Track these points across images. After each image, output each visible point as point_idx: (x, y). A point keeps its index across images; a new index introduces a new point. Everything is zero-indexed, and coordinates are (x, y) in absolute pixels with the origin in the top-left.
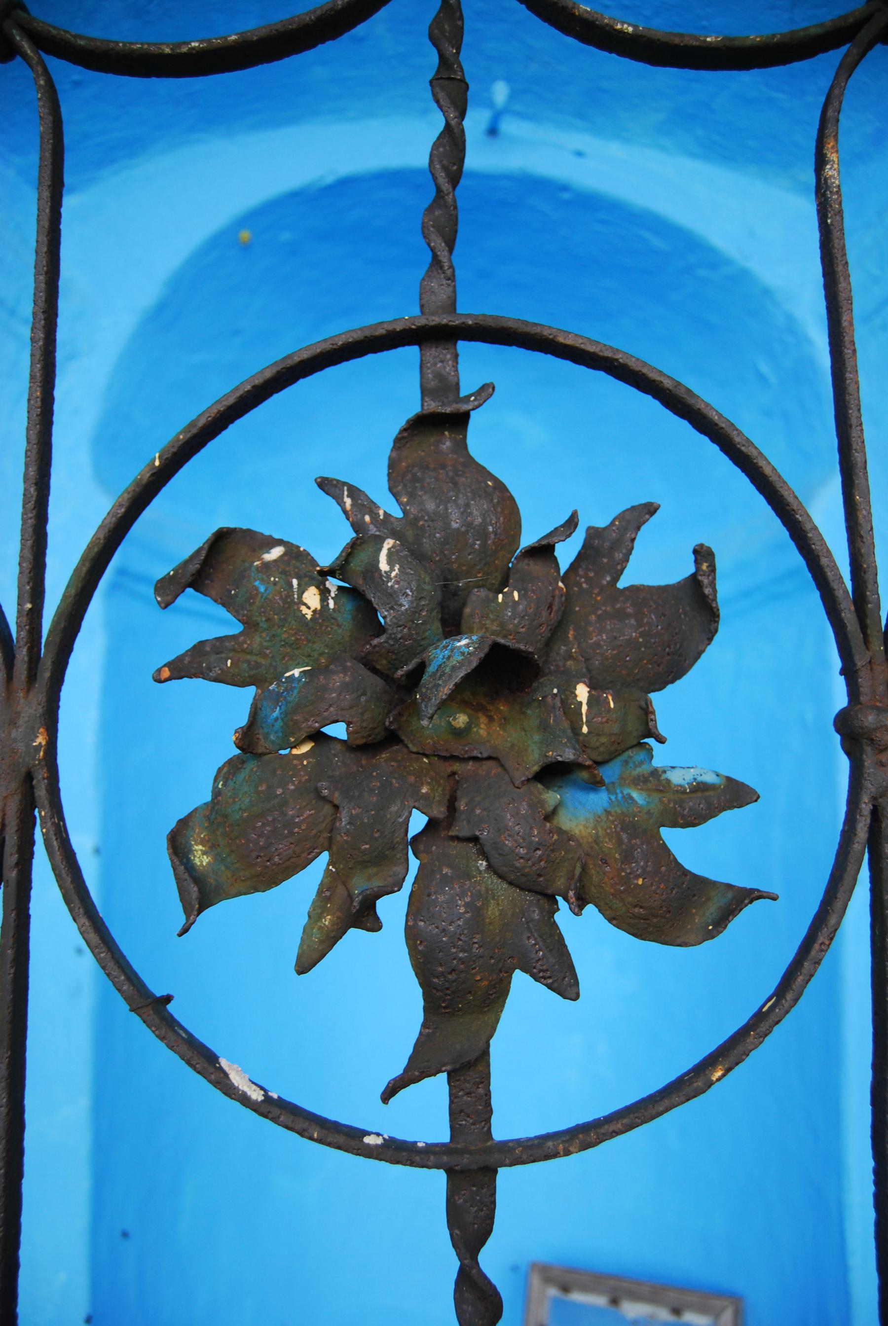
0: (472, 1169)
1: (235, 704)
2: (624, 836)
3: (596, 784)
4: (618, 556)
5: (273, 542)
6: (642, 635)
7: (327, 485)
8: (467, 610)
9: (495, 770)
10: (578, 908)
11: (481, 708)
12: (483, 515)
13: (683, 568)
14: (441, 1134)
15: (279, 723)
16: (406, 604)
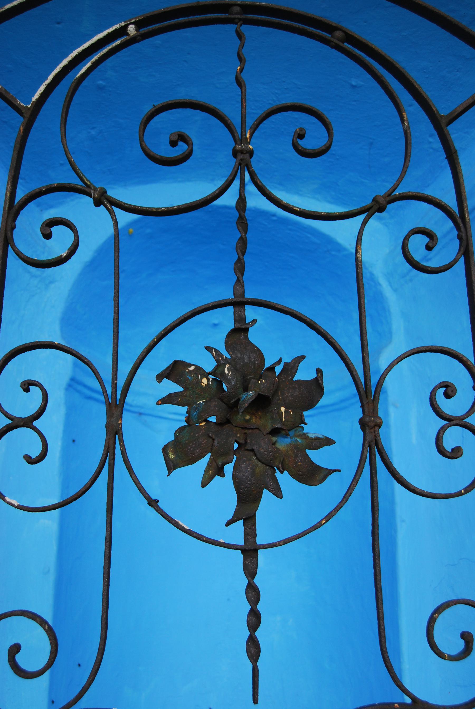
0: (250, 551)
1: (181, 412)
2: (295, 450)
3: (287, 435)
4: (294, 371)
5: (191, 365)
6: (300, 394)
7: (208, 348)
8: (250, 385)
9: (257, 431)
10: (282, 472)
11: (254, 415)
12: (254, 358)
13: (312, 375)
14: (242, 542)
15: (196, 416)
16: (233, 383)
